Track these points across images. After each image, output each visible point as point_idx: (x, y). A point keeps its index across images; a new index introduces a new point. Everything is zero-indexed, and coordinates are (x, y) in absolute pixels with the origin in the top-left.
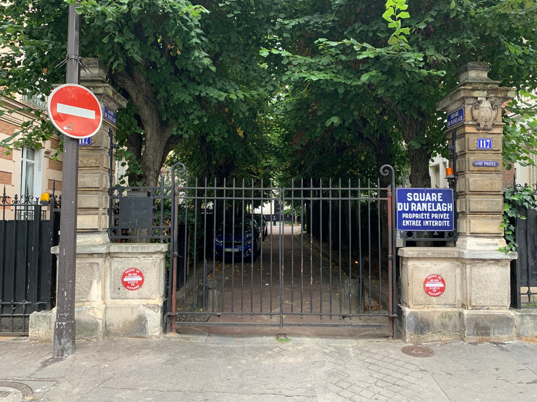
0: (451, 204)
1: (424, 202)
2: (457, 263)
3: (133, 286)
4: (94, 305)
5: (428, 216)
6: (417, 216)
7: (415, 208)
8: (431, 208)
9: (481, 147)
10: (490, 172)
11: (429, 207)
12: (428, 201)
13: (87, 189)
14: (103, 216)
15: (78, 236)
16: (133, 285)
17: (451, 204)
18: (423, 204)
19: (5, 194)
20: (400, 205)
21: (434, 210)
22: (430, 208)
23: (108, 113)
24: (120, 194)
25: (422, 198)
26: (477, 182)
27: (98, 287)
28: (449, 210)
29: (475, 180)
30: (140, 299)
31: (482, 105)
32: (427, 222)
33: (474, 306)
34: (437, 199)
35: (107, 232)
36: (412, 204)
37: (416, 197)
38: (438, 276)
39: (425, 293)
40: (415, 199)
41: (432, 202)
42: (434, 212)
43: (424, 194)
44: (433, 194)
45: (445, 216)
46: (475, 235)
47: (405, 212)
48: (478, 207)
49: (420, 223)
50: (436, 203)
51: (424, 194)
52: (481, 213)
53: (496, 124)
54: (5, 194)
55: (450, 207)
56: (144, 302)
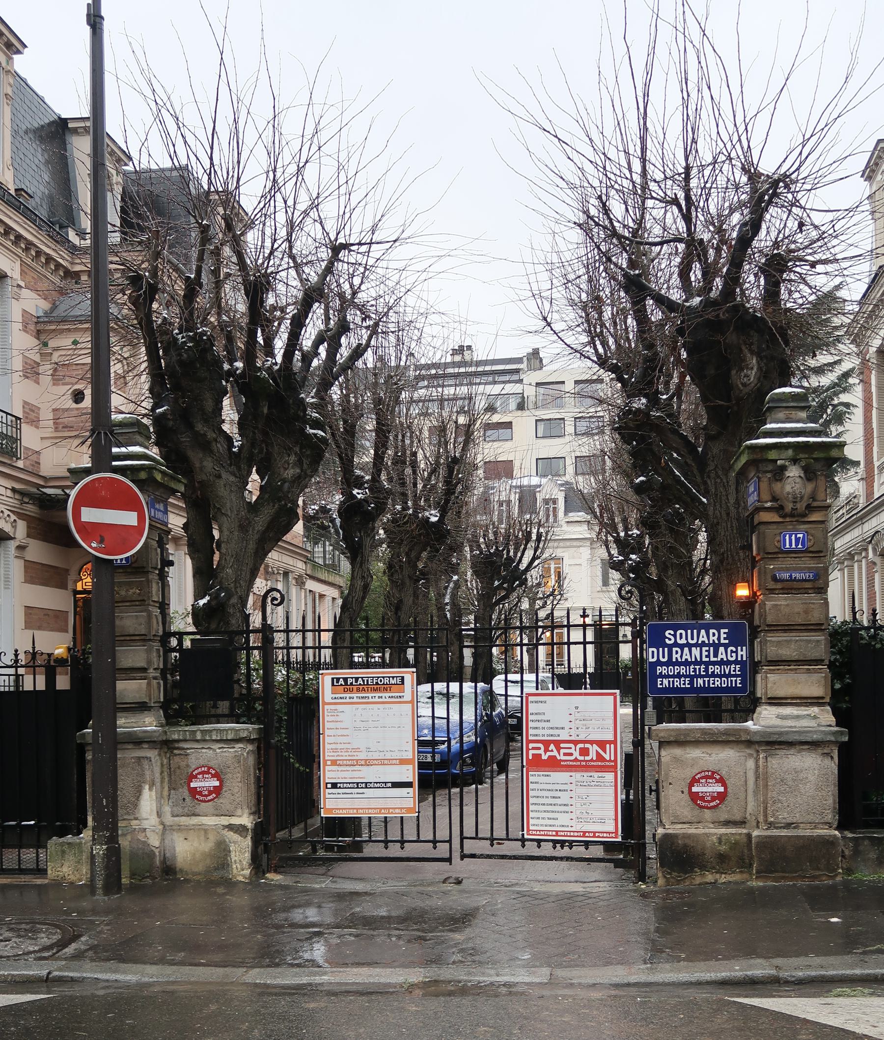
0: (744, 648)
1: (696, 645)
2: (748, 751)
3: (206, 796)
4: (146, 824)
5: (702, 670)
6: (682, 670)
7: (678, 656)
8: (708, 656)
9: (788, 546)
10: (806, 591)
11: (705, 653)
12: (703, 644)
13: (128, 638)
14: (155, 681)
15: (119, 714)
16: (206, 793)
17: (744, 648)
18: (693, 649)
19: (34, 648)
20: (653, 652)
21: (712, 659)
22: (707, 656)
23: (155, 509)
24: (180, 643)
25: (692, 639)
26: (780, 610)
27: (150, 796)
28: (739, 659)
29: (777, 605)
30: (217, 816)
31: (787, 474)
32: (700, 681)
33: (771, 823)
34: (719, 639)
35: (161, 707)
36: (674, 649)
37: (681, 638)
38: (713, 773)
39: (690, 803)
40: (679, 641)
41: (709, 645)
42: (714, 663)
43: (695, 631)
44: (711, 631)
45: (732, 669)
46: (776, 701)
47: (662, 664)
48: (780, 652)
49: (687, 682)
50: (716, 646)
51: (695, 631)
52: (788, 662)
53: (815, 504)
54: (34, 648)
55: (743, 653)
56: (225, 821)
